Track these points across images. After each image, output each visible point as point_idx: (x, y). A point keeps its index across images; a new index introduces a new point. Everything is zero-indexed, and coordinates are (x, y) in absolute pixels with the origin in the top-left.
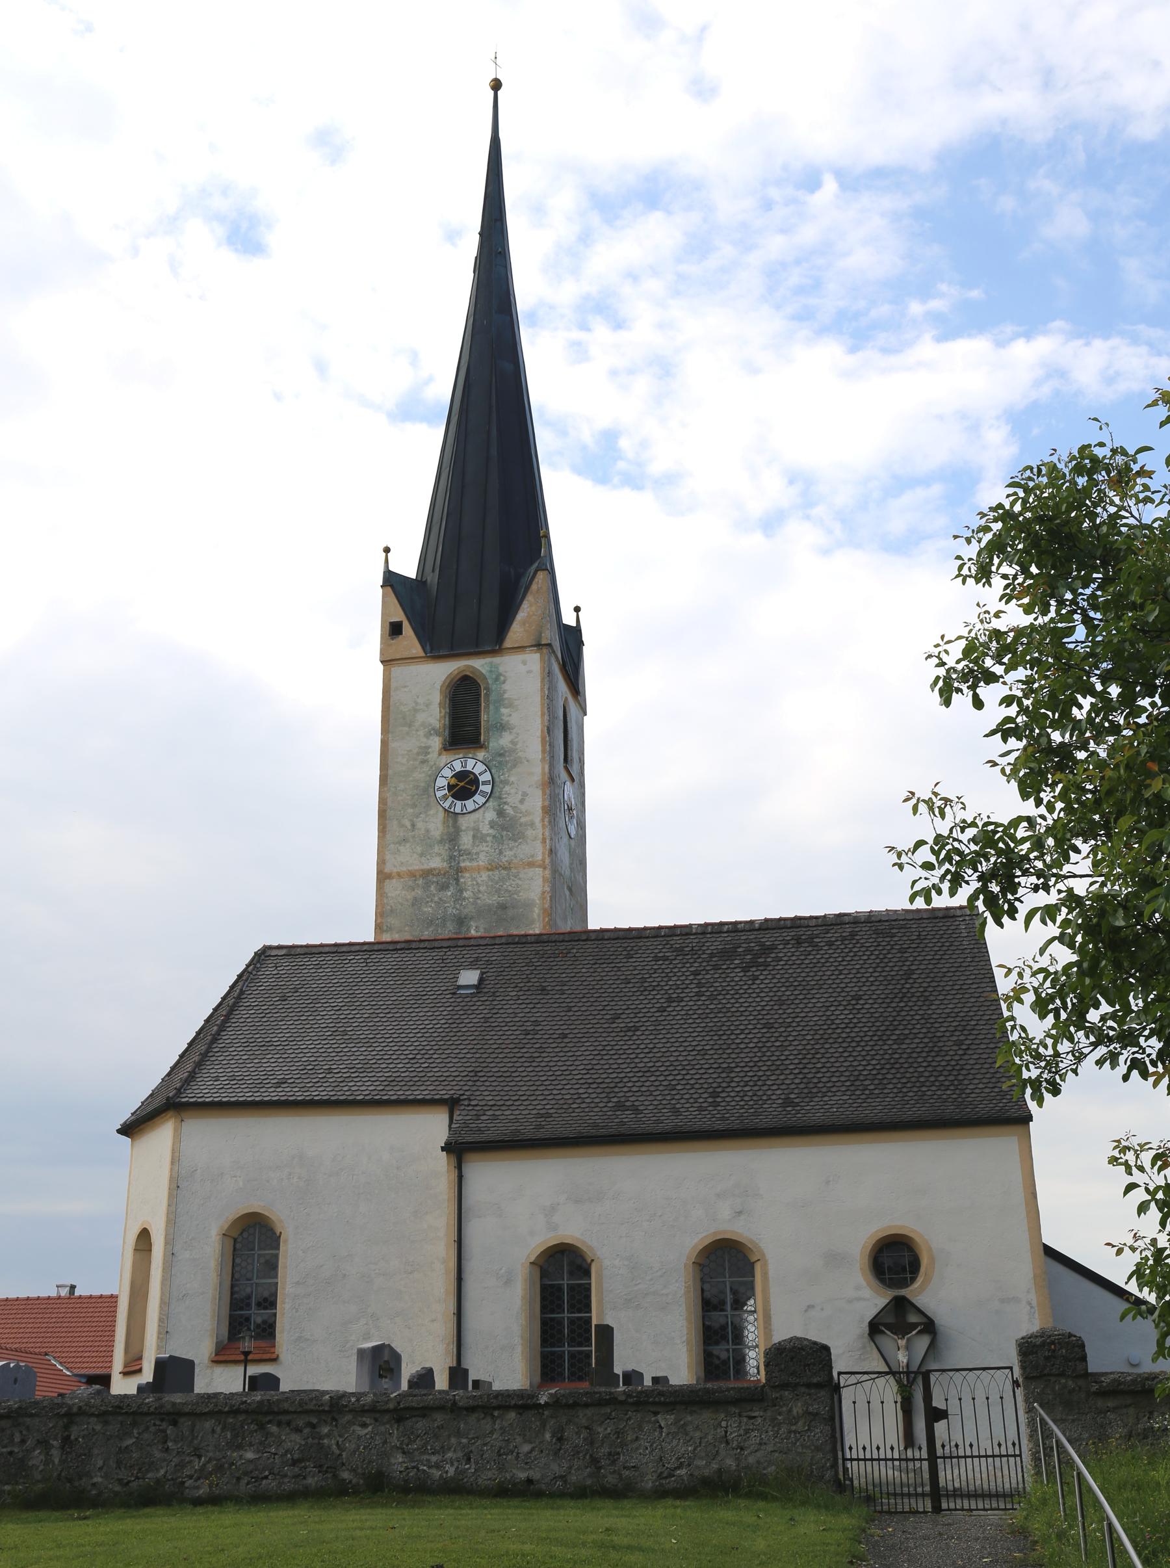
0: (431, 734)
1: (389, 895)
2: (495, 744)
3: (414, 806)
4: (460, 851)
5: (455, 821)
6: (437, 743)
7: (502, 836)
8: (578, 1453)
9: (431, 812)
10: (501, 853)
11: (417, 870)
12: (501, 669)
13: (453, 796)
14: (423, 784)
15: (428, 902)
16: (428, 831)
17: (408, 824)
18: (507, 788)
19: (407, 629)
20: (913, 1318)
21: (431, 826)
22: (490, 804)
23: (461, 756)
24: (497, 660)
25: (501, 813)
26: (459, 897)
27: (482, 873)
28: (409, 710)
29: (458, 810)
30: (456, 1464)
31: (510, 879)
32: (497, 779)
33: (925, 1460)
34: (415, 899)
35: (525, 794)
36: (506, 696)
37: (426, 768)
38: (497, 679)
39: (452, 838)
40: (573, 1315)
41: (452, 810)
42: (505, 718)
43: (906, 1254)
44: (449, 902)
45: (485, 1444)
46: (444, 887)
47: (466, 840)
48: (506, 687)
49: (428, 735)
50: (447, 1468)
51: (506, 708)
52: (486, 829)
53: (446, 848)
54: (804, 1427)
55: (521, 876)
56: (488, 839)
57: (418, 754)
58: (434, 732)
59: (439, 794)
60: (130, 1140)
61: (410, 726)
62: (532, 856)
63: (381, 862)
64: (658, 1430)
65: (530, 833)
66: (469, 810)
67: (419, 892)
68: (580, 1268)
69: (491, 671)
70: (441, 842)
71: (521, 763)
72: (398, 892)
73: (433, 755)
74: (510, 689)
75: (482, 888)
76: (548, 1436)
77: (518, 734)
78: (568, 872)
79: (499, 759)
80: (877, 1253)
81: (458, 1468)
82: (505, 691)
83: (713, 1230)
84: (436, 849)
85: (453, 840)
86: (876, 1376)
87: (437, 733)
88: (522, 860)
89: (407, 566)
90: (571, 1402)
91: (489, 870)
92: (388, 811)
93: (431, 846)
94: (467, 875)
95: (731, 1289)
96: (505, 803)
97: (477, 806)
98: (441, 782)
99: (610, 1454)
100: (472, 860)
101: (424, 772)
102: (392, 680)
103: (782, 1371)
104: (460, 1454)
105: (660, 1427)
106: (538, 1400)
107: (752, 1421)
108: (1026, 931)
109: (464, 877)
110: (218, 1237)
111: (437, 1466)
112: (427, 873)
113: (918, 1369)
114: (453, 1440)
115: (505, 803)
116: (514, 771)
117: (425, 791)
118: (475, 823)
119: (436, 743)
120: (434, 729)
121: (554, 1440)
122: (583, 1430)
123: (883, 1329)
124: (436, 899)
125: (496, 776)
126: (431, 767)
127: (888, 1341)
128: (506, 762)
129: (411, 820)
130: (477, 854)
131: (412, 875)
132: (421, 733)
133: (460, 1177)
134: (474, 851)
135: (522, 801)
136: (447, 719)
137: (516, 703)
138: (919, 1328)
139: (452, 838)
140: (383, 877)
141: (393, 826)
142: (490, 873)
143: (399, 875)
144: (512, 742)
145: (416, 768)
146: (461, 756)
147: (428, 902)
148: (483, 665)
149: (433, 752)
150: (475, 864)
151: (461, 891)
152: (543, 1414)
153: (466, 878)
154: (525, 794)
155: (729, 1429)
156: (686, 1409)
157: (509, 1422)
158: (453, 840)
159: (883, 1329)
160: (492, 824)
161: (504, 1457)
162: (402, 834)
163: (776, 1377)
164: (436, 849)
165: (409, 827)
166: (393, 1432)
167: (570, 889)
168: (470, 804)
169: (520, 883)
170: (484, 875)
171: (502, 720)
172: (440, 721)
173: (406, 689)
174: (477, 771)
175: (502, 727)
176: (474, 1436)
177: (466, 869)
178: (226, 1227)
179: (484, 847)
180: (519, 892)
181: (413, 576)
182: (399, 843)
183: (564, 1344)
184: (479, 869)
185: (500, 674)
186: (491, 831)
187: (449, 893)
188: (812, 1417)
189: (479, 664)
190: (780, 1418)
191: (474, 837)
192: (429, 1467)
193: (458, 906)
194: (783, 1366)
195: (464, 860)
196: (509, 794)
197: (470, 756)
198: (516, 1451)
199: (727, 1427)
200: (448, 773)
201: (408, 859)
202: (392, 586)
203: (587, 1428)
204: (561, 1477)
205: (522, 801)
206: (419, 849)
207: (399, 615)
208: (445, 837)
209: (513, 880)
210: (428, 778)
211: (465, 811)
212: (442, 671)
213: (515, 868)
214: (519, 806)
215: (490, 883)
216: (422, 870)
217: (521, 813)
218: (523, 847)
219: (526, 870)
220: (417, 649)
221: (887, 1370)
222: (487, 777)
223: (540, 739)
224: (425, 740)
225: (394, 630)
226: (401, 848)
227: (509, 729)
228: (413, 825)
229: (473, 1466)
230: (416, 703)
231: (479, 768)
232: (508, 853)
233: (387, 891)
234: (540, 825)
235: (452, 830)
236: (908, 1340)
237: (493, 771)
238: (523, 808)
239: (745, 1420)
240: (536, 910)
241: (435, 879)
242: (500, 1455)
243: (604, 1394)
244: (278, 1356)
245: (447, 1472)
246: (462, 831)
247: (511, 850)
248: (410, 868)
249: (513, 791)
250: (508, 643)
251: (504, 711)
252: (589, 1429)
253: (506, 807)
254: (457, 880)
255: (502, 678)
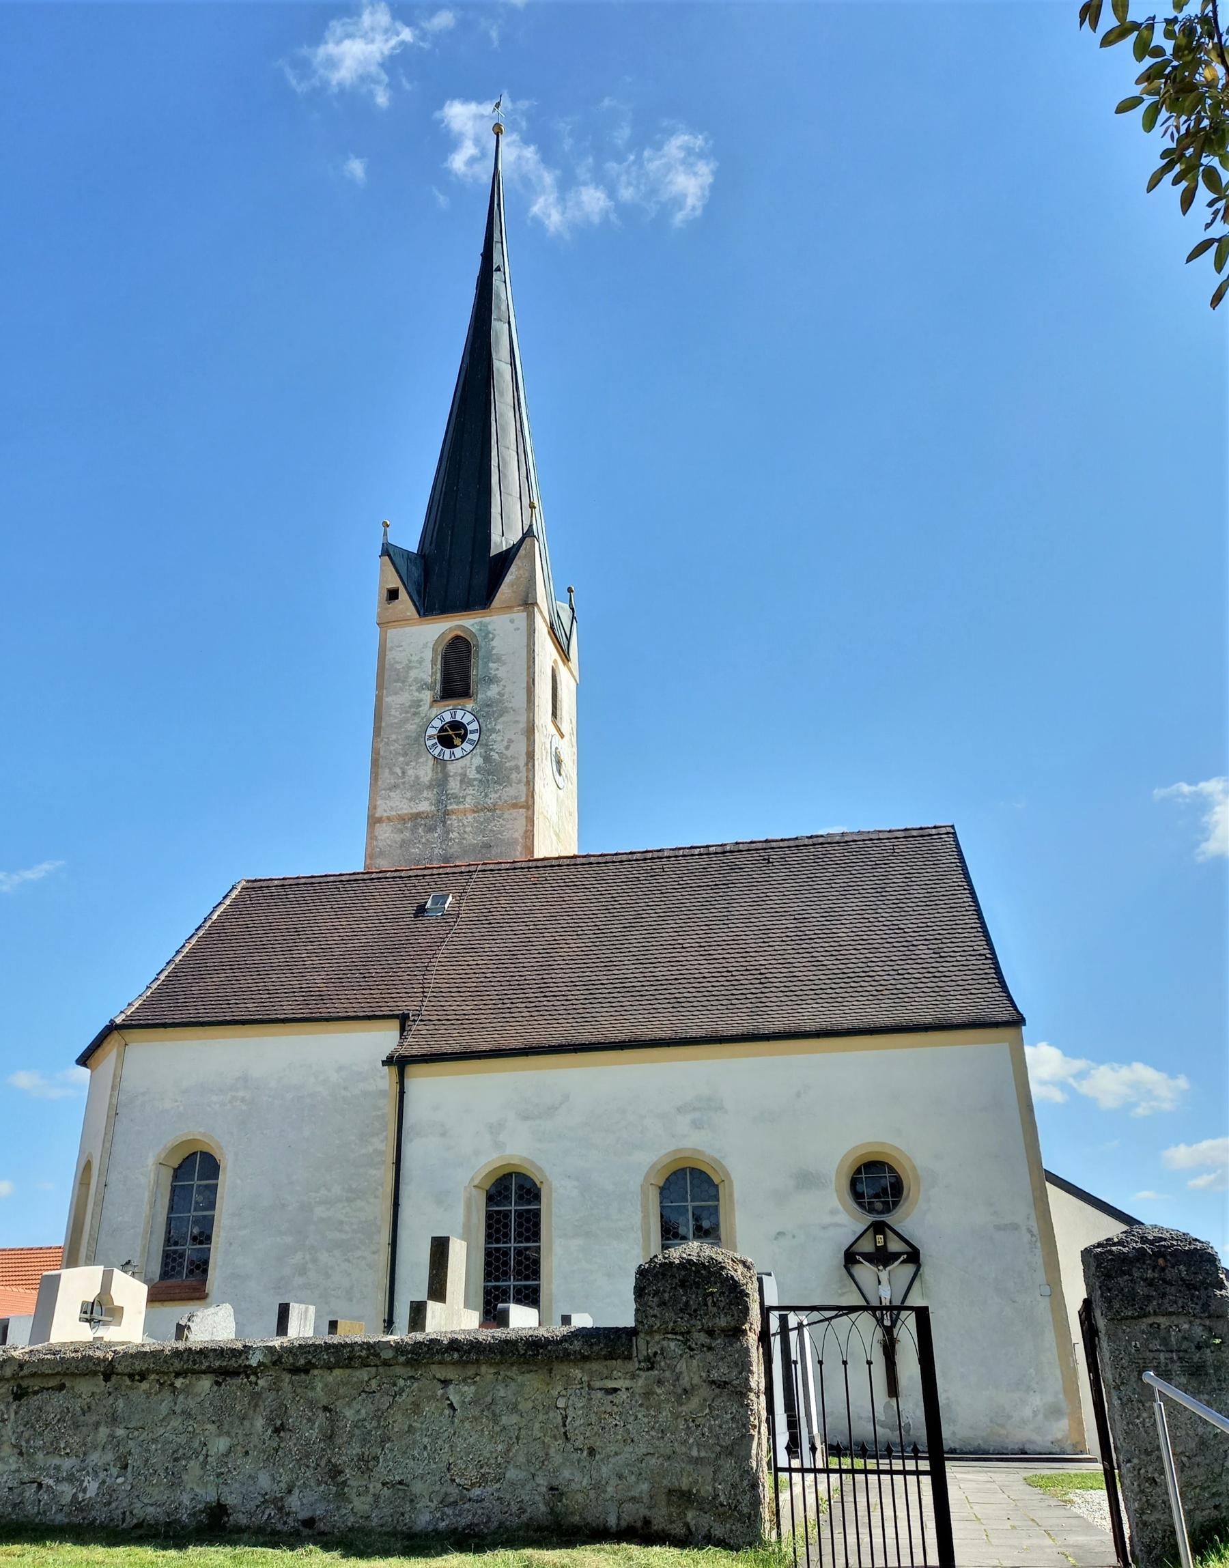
0: (423, 689)
1: (379, 838)
2: (484, 696)
3: (405, 754)
4: (447, 795)
5: (444, 767)
6: (429, 697)
7: (488, 781)
8: (308, 1456)
9: (421, 760)
10: (486, 796)
11: (406, 814)
12: (490, 628)
13: (439, 738)
14: (414, 735)
15: (415, 843)
16: (417, 777)
17: (398, 771)
18: (493, 736)
19: (403, 594)
20: (895, 1246)
21: (421, 773)
22: (477, 751)
23: (451, 708)
24: (486, 620)
25: (487, 759)
26: (445, 838)
27: (467, 815)
28: (403, 668)
29: (447, 757)
30: (102, 1475)
31: (494, 820)
32: (484, 728)
33: (925, 1473)
34: (403, 840)
35: (510, 741)
36: (494, 652)
37: (417, 721)
38: (486, 636)
39: (440, 783)
40: (521, 1245)
41: (441, 758)
42: (493, 672)
43: (887, 1175)
44: (435, 843)
45: (154, 1441)
46: (431, 829)
47: (454, 785)
48: (493, 643)
49: (420, 689)
50: (85, 1484)
51: (494, 663)
52: (472, 774)
53: (435, 792)
54: (702, 1411)
55: (505, 816)
56: (475, 783)
57: (410, 707)
58: (431, 687)
59: (429, 743)
60: (88, 1071)
61: (403, 682)
62: (516, 798)
63: (373, 807)
64: (447, 1412)
65: (514, 776)
66: (457, 757)
67: (407, 834)
68: (529, 1192)
69: (481, 630)
70: (430, 787)
71: (507, 712)
72: (387, 835)
73: (424, 708)
74: (498, 646)
75: (467, 830)
76: (259, 1423)
77: (505, 686)
78: (555, 819)
79: (486, 709)
80: (854, 1174)
81: (104, 1482)
82: (493, 648)
83: (672, 1148)
84: (425, 794)
85: (441, 785)
86: (833, 1313)
87: (431, 687)
88: (506, 801)
89: (410, 540)
90: (302, 1361)
91: (474, 812)
92: (381, 760)
93: (421, 791)
94: (454, 817)
95: (693, 1215)
96: (492, 750)
97: (465, 753)
98: (432, 731)
99: (361, 1458)
100: (458, 803)
101: (415, 723)
102: (388, 640)
103: (665, 1304)
104: (109, 1456)
105: (451, 1406)
106: (247, 1359)
107: (610, 1397)
108: (1149, 190)
109: (451, 819)
110: (154, 1167)
111: (71, 1478)
112: (416, 817)
113: (903, 1301)
114: (103, 1431)
115: (492, 750)
116: (501, 720)
117: (416, 740)
118: (462, 768)
119: (427, 696)
120: (425, 684)
121: (269, 1432)
122: (321, 1414)
123: (861, 1260)
124: (424, 840)
125: (483, 726)
126: (423, 719)
127: (865, 1271)
128: (493, 711)
129: (401, 768)
130: (464, 797)
131: (402, 819)
132: (414, 688)
133: (402, 1093)
134: (461, 795)
135: (507, 748)
136: (439, 675)
137: (503, 658)
138: (902, 1259)
139: (440, 783)
140: (374, 821)
141: (385, 775)
142: (476, 815)
143: (389, 819)
144: (499, 693)
145: (408, 720)
146: (451, 708)
147: (415, 843)
148: (473, 625)
149: (424, 704)
150: (462, 807)
151: (447, 832)
152: (256, 1384)
153: (453, 821)
154: (510, 741)
155: (571, 1413)
156: (497, 1373)
157: (199, 1400)
158: (441, 785)
159: (861, 1260)
160: (479, 769)
161: (184, 1463)
162: (392, 781)
163: (655, 1316)
164: (425, 794)
165: (400, 775)
166: (9, 1418)
167: (557, 835)
168: (458, 752)
169: (504, 823)
170: (470, 818)
171: (490, 673)
172: (432, 677)
173: (400, 649)
174: (465, 721)
175: (490, 680)
176: (139, 1424)
177: (453, 812)
178: (163, 1156)
179: (470, 791)
180: (504, 831)
181: (416, 552)
182: (390, 789)
183: (510, 1277)
184: (465, 812)
185: (489, 633)
186: (478, 776)
187: (436, 835)
188: (717, 1391)
189: (467, 622)
190: (659, 1391)
191: (461, 782)
192: (58, 1481)
193: (444, 847)
194: (666, 1296)
195: (451, 804)
196: (495, 742)
197: (460, 707)
198: (204, 1452)
199: (567, 1407)
200: (438, 724)
201: (397, 804)
202: (389, 556)
203: (326, 1409)
204: (275, 1501)
205: (507, 748)
206: (408, 795)
207: (395, 583)
208: (434, 783)
209: (498, 821)
210: (419, 729)
211: (453, 758)
212: (439, 628)
213: (500, 810)
214: (505, 752)
215: (475, 825)
216: (411, 814)
217: (506, 758)
218: (507, 789)
219: (511, 811)
220: (411, 611)
221: (863, 1303)
222: (475, 726)
223: (525, 690)
224: (417, 694)
225: (393, 595)
226: (392, 794)
227: (497, 682)
228: (403, 773)
229: (130, 1480)
230: (410, 661)
231: (467, 719)
232: (493, 796)
233: (377, 834)
234: (525, 769)
235: (440, 775)
236: (889, 1272)
237: (480, 721)
238: (508, 753)
239: (599, 1394)
240: (519, 848)
241: (423, 822)
242: (176, 1460)
243: (357, 1348)
244: (208, 1294)
245: (85, 1491)
246: (450, 776)
247: (496, 792)
248: (399, 813)
249: (499, 739)
250: (496, 602)
251: (491, 665)
252: (330, 1411)
253: (492, 753)
254: (444, 822)
255: (491, 636)
